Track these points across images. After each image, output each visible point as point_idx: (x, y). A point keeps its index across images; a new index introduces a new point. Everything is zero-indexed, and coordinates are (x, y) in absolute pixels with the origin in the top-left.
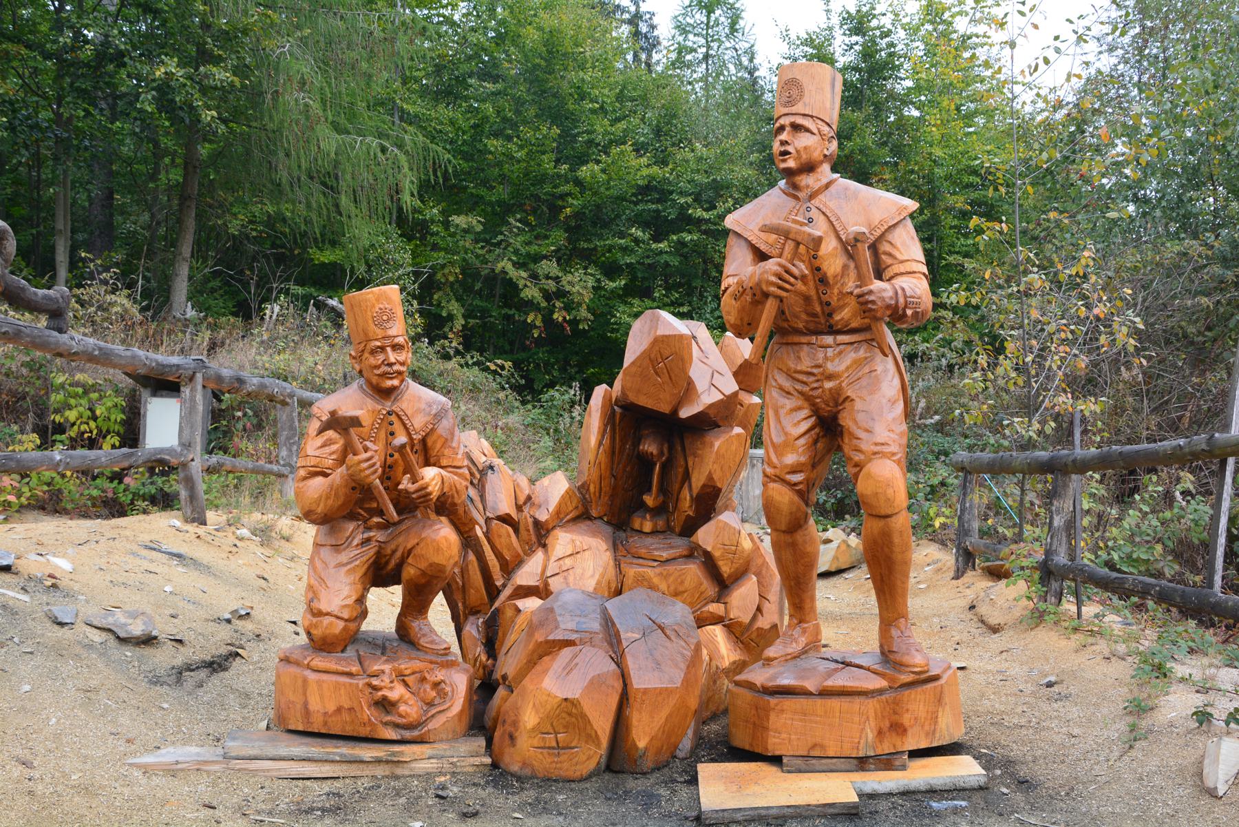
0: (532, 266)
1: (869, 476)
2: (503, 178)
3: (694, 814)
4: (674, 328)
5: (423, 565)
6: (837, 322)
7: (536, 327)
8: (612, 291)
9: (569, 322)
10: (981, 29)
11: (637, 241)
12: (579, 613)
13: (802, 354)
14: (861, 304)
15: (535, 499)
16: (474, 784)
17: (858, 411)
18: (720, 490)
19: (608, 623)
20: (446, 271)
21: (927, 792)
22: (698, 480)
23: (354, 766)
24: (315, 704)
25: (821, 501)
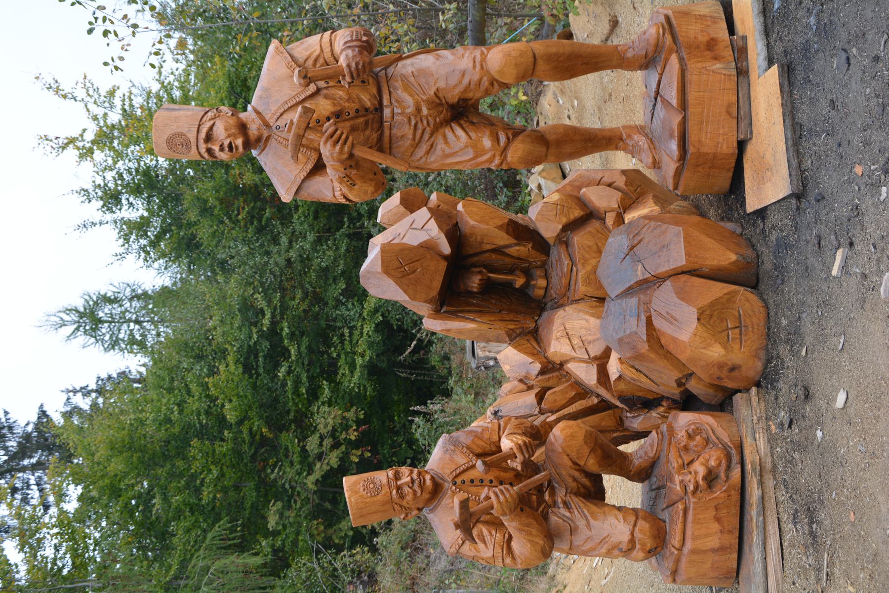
0: (311, 459)
1: (501, 72)
2: (237, 488)
3: (794, 201)
5: (586, 450)
6: (372, 104)
7: (362, 454)
8: (332, 392)
9: (358, 426)
10: (117, 102)
11: (289, 373)
12: (622, 317)
13: (400, 134)
15: (523, 374)
16: (776, 399)
17: (447, 84)
19: (629, 292)
20: (315, 532)
21: (765, 16)
22: (503, 239)
23: (767, 505)
24: (713, 542)
25: (506, 199)
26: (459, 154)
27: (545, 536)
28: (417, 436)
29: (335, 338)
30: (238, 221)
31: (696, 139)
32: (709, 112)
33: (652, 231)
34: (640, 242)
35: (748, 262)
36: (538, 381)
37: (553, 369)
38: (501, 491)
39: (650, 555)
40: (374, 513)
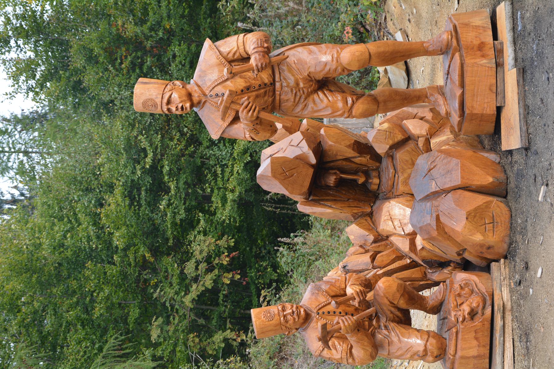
1: (349, 64)
4: (267, 166)
5: (398, 295)
6: (269, 81)
7: (233, 277)
11: (168, 205)
14: (262, 69)
16: (514, 267)
17: (315, 70)
18: (356, 141)
21: (514, 32)
22: (350, 153)
23: (506, 330)
24: (473, 352)
25: (359, 75)
26: (323, 110)
27: (373, 346)
28: (282, 263)
29: (209, 175)
30: (122, 69)
31: (470, 105)
32: (478, 89)
33: (442, 161)
34: (434, 167)
35: (500, 183)
36: (372, 247)
37: (382, 240)
38: (346, 319)
39: (436, 359)
40: (270, 331)
